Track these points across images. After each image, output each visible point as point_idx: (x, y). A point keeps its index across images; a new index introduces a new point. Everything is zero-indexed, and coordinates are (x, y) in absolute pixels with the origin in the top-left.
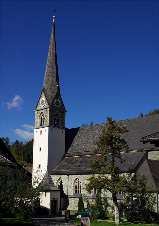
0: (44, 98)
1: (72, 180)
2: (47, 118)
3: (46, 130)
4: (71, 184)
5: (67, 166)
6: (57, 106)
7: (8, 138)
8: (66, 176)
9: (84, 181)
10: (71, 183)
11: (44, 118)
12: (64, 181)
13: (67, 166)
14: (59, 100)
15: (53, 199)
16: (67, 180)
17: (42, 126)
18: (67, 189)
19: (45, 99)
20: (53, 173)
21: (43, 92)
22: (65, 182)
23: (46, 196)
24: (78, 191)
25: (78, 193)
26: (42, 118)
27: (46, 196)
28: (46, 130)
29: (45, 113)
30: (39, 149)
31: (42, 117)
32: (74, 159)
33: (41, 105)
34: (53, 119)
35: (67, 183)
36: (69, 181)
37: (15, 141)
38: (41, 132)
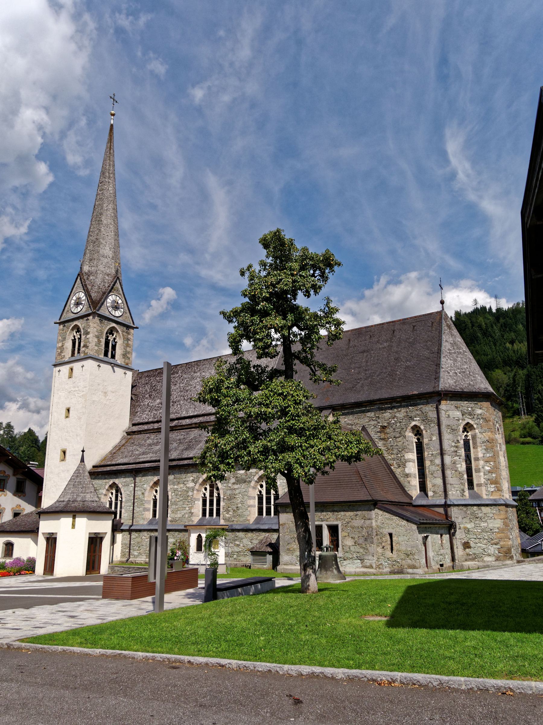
0: (81, 293)
1: (145, 486)
2: (88, 336)
3: (82, 367)
4: (141, 496)
5: (134, 452)
6: (113, 312)
7: (12, 424)
8: (129, 480)
9: (176, 487)
10: (143, 494)
11: (80, 339)
12: (126, 488)
13: (134, 452)
14: (118, 298)
15: (93, 536)
16: (133, 485)
17: (74, 358)
18: (132, 507)
19: (83, 294)
20: (109, 315)
21: (79, 280)
22: (128, 492)
23: (73, 526)
24: (211, 511)
25: (210, 516)
26: (76, 338)
27: (73, 526)
28: (82, 367)
29: (83, 326)
30: (64, 411)
31: (74, 337)
32: (152, 438)
33: (72, 308)
34: (103, 341)
35: (133, 493)
36: (136, 489)
37: (26, 430)
38: (72, 369)
